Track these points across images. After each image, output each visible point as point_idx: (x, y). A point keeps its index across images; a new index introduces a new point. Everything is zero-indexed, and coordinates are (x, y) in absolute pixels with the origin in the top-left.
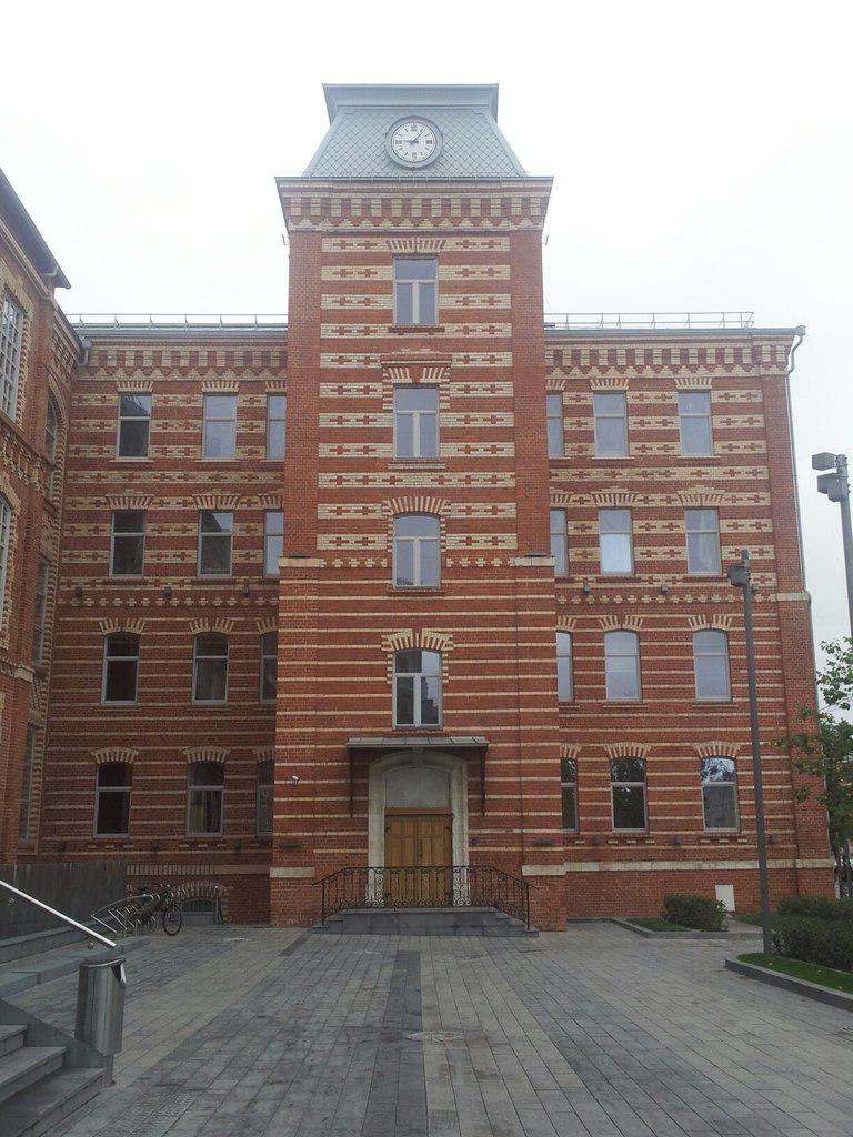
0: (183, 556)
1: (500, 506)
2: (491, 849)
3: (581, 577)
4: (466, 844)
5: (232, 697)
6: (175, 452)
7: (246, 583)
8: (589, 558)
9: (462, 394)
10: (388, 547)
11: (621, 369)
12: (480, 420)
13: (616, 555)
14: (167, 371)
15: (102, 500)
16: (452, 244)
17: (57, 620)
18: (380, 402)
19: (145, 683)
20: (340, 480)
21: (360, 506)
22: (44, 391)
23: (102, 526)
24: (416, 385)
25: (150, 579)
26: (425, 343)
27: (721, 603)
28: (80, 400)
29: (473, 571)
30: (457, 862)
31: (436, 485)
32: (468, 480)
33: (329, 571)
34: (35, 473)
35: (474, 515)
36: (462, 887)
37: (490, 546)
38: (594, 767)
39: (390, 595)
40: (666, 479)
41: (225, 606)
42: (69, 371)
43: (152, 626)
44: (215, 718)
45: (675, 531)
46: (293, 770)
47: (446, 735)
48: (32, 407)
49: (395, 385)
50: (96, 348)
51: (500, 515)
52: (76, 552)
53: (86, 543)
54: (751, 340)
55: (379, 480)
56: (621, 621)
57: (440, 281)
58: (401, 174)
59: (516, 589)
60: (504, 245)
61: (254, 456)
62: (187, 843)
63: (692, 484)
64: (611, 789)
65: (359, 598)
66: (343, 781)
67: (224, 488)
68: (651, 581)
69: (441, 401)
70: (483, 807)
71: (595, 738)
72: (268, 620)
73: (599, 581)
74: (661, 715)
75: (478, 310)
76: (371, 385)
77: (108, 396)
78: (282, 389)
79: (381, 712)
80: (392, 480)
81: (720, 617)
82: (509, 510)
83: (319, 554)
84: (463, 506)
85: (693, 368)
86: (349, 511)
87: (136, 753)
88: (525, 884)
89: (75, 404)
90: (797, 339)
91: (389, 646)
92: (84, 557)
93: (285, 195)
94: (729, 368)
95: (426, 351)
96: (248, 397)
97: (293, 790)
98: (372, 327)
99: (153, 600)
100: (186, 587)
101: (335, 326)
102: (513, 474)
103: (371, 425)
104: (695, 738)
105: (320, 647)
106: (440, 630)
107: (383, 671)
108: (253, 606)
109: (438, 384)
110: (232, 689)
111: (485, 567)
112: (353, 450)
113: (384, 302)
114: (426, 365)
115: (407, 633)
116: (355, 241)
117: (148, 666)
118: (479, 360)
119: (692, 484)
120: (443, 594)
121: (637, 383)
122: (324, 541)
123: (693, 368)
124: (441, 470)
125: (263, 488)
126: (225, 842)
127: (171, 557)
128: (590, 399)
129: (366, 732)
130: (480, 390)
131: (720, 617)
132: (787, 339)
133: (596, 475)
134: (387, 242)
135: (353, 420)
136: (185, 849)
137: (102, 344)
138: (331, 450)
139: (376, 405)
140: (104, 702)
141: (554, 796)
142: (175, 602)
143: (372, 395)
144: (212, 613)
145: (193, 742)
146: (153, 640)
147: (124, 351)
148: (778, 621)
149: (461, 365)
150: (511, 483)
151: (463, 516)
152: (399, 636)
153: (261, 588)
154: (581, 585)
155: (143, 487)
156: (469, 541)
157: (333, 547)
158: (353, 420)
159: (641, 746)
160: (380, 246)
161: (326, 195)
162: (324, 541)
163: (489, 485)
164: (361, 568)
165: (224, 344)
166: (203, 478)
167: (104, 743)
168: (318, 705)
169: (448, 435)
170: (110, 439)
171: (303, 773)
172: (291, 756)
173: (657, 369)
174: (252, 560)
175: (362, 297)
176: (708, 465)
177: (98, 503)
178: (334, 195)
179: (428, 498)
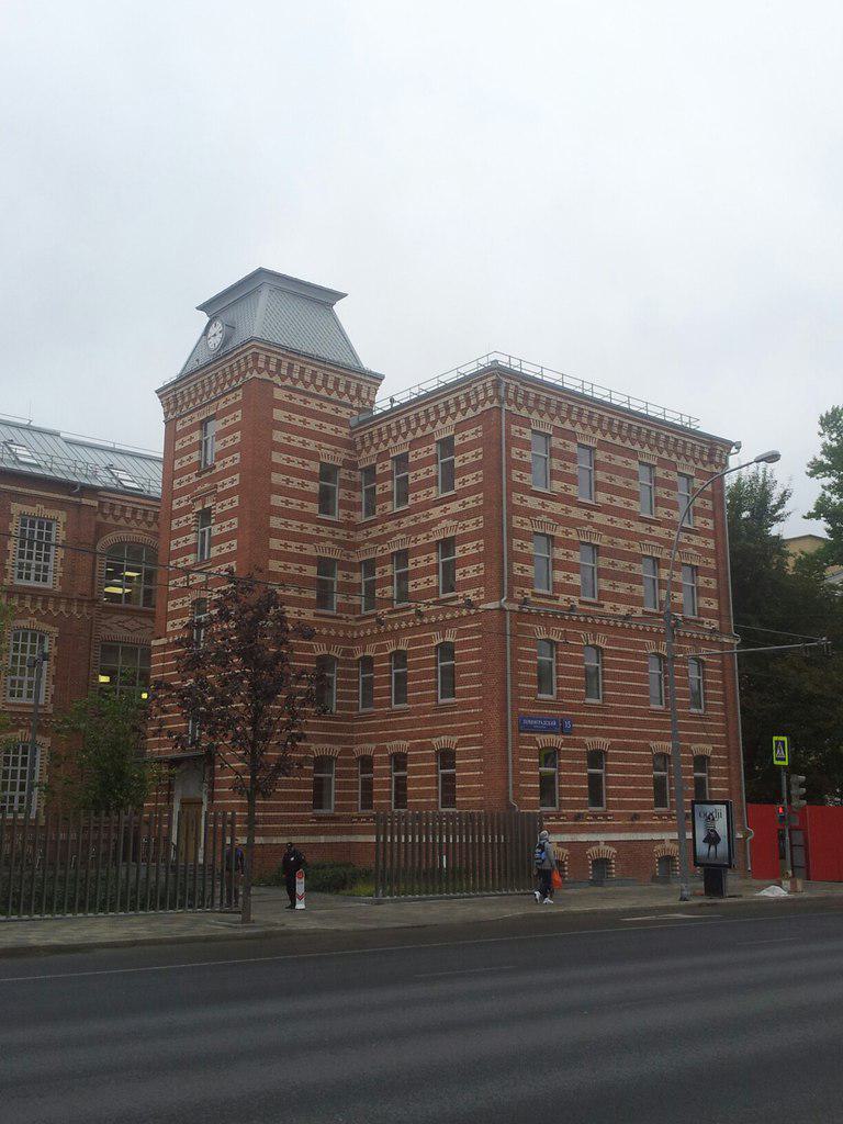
27: (452, 619)
43: (413, 642)
104: (433, 734)
117: (414, 675)
170: (343, 505)
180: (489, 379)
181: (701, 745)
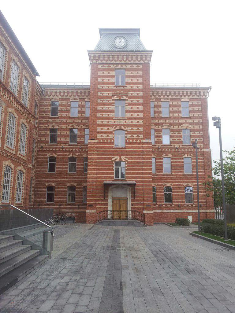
1: (139, 128)
3: (158, 145)
7: (81, 145)
9: (131, 102)
11: (168, 96)
12: (135, 108)
14: (62, 96)
16: (129, 67)
18: (112, 103)
19: (57, 168)
22: (34, 100)
24: (120, 100)
25: (59, 144)
26: (122, 90)
28: (42, 102)
29: (133, 143)
30: (128, 209)
31: (124, 123)
34: (32, 120)
35: (133, 130)
36: (130, 215)
37: (137, 137)
38: (160, 188)
39: (114, 148)
43: (59, 155)
51: (139, 130)
55: (111, 122)
56: (167, 155)
58: (117, 50)
59: (143, 147)
61: (82, 116)
63: (184, 123)
64: (164, 194)
66: (103, 191)
67: (75, 123)
71: (161, 182)
73: (162, 146)
76: (110, 100)
82: (141, 129)
83: (97, 139)
84: (131, 128)
85: (185, 96)
88: (144, 215)
89: (41, 103)
90: (209, 89)
92: (43, 139)
93: (90, 55)
95: (122, 92)
96: (81, 102)
97: (91, 193)
98: (110, 86)
100: (67, 146)
101: (101, 86)
104: (184, 182)
107: (112, 166)
108: (82, 151)
112: (105, 115)
113: (112, 80)
115: (117, 157)
118: (135, 94)
119: (184, 123)
120: (126, 148)
123: (185, 96)
127: (63, 139)
130: (135, 101)
132: (207, 90)
133: (162, 121)
134: (114, 66)
135: (105, 108)
139: (111, 104)
142: (64, 150)
143: (110, 102)
144: (72, 152)
145: (69, 182)
146: (59, 158)
149: (131, 95)
150: (142, 123)
151: (131, 130)
154: (158, 147)
155: (57, 123)
156: (132, 136)
157: (100, 137)
158: (105, 108)
160: (112, 67)
162: (98, 136)
163: (137, 123)
166: (71, 121)
171: (93, 189)
174: (82, 140)
175: (108, 79)
176: (188, 119)
178: (101, 55)
180: (54, 90)
181: (73, 183)
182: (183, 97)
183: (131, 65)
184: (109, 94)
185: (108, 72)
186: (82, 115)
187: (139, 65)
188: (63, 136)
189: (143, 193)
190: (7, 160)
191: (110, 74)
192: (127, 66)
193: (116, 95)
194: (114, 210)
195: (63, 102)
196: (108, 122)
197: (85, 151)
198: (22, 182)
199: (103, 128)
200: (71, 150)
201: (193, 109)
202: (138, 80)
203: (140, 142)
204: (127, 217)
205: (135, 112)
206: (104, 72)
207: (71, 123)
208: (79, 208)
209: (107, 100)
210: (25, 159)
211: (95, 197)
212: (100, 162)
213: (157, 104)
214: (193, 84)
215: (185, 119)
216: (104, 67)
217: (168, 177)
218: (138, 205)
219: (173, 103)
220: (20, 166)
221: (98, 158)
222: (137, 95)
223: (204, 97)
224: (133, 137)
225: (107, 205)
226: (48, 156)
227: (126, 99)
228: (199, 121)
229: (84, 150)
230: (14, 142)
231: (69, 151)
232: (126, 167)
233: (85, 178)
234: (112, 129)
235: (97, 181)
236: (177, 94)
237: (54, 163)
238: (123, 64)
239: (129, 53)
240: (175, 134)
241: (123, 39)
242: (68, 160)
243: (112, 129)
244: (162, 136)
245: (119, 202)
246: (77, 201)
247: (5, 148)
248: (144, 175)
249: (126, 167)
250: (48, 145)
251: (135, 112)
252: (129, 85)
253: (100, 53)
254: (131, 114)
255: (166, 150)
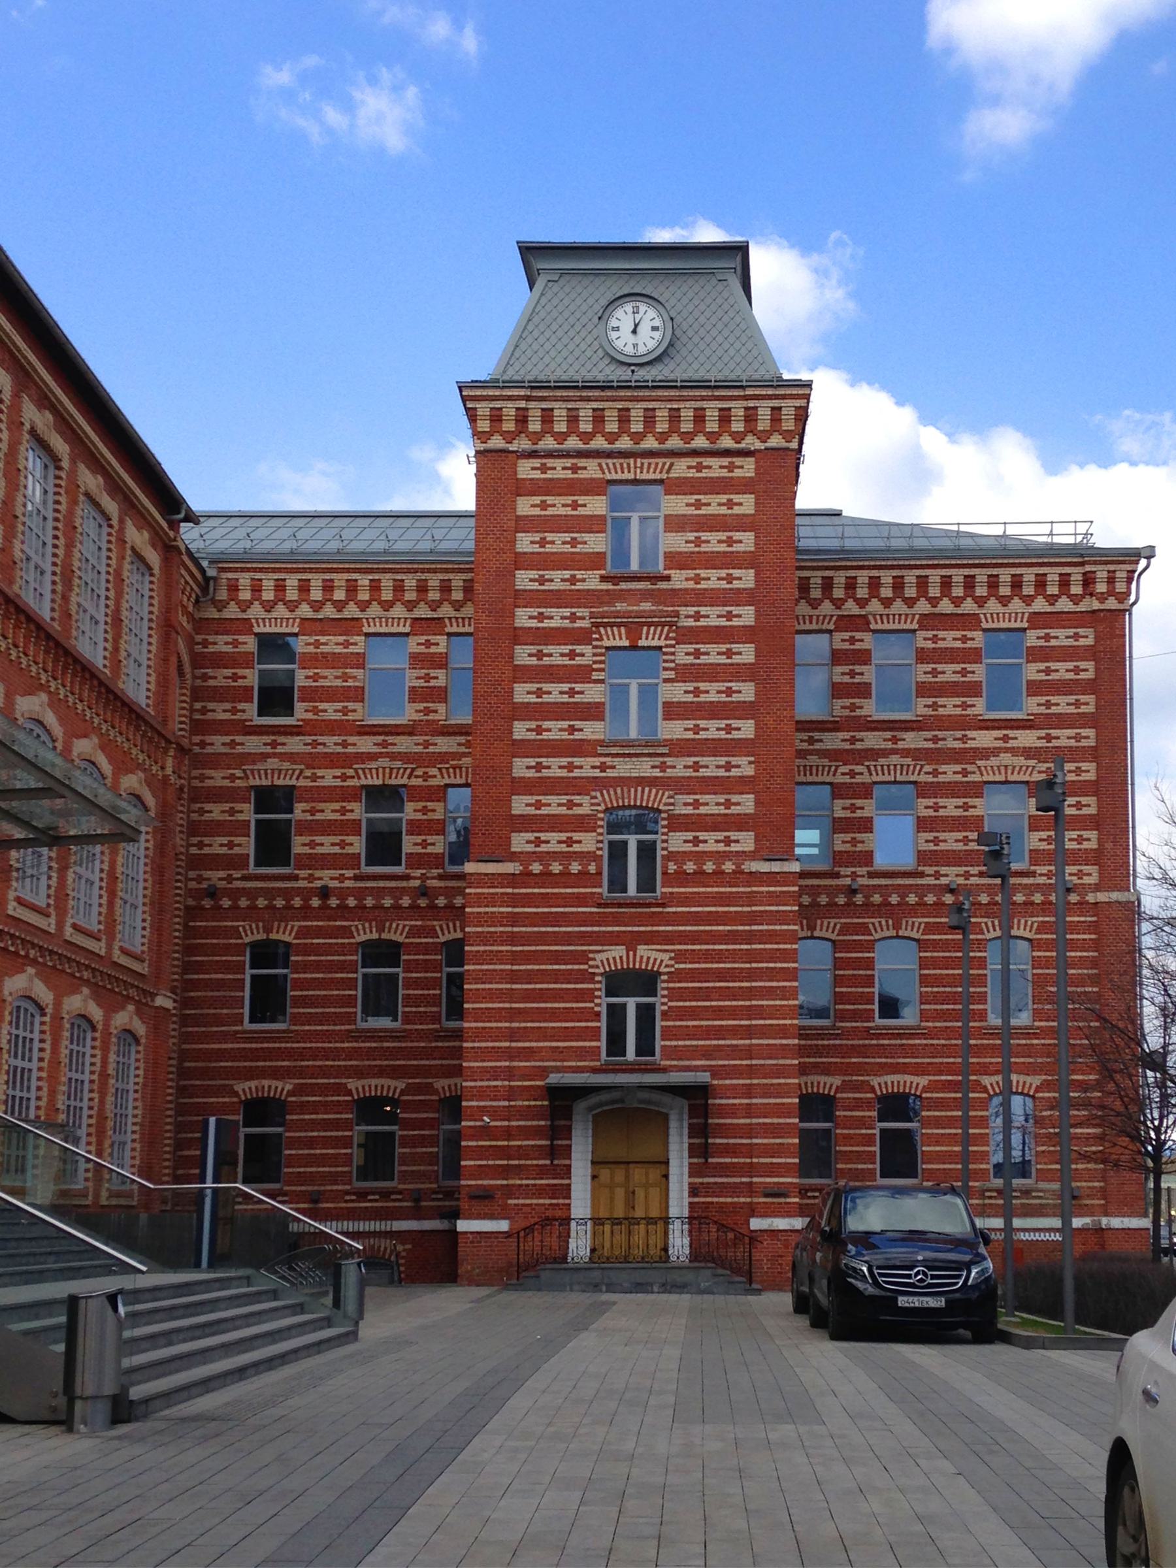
0: (342, 844)
1: (735, 798)
2: (715, 1200)
3: (849, 871)
4: (686, 1194)
5: (407, 1019)
6: (331, 711)
7: (423, 878)
8: (860, 847)
9: (690, 660)
10: (598, 849)
11: (910, 602)
12: (712, 692)
13: (893, 842)
14: (317, 606)
15: (238, 773)
16: (682, 468)
17: (186, 926)
18: (589, 669)
19: (298, 1002)
20: (539, 767)
21: (564, 799)
22: (174, 659)
23: (238, 806)
24: (634, 647)
25: (303, 873)
26: (646, 595)
27: (1025, 903)
28: (205, 644)
29: (700, 876)
30: (673, 1212)
31: (657, 773)
32: (696, 767)
33: (526, 877)
34: (169, 763)
35: (703, 810)
36: (679, 1243)
37: (721, 847)
38: (858, 1104)
39: (599, 905)
40: (962, 746)
41: (397, 907)
42: (191, 609)
44: (386, 1044)
45: (971, 812)
46: (483, 1110)
47: (664, 1070)
48: (163, 684)
49: (607, 648)
50: (224, 575)
51: (735, 810)
52: (207, 840)
53: (216, 828)
54: (1082, 564)
55: (587, 767)
56: (897, 927)
57: (666, 516)
58: (624, 374)
59: (751, 899)
60: (747, 468)
61: (431, 717)
62: (354, 1194)
63: (995, 752)
64: (877, 1132)
65: (561, 910)
66: (542, 1123)
67: (393, 757)
68: (937, 875)
69: (665, 669)
70: (706, 1152)
71: (859, 1069)
72: (451, 925)
73: (871, 875)
74: (943, 1042)
75: (712, 552)
76: (579, 649)
77: (241, 638)
78: (467, 629)
79: (587, 1044)
80: (603, 767)
81: (1023, 921)
82: (746, 804)
83: (513, 857)
84: (690, 799)
85: (1004, 601)
86: (549, 805)
87: (288, 1087)
88: (754, 1238)
89: (198, 648)
90: (1143, 562)
91: (597, 967)
92: (217, 845)
93: (469, 405)
94: (1051, 600)
95: (646, 606)
96: (422, 639)
97: (485, 1132)
98: (579, 574)
99: (306, 899)
100: (348, 884)
101: (534, 574)
102: (752, 759)
103: (578, 698)
105: (515, 967)
106: (659, 947)
107: (589, 995)
108: (432, 907)
109: (660, 648)
110: (407, 1009)
111: (715, 873)
112: (555, 730)
113: (595, 543)
114: (644, 624)
115: (618, 951)
116: (558, 463)
118: (713, 617)
119: (995, 752)
120: (663, 905)
121: (929, 621)
122: (520, 842)
123: (1004, 601)
124: (662, 755)
125: (443, 757)
126: (400, 1192)
127: (327, 845)
128: (867, 641)
129: (570, 1067)
130: (713, 655)
131: (1023, 921)
132: (1131, 562)
133: (873, 740)
134: (600, 465)
135: (555, 693)
136: (352, 1201)
137: (230, 570)
138: (528, 730)
139: (583, 674)
140: (247, 1025)
141: (790, 1141)
142: (334, 902)
143: (579, 661)
144: (379, 917)
145: (359, 1073)
146: (307, 950)
147: (260, 580)
148: (1093, 927)
149: (690, 623)
150: (749, 771)
151: (689, 810)
152: (610, 955)
153: (442, 884)
154: (848, 881)
155: (291, 757)
156: (696, 841)
157: (530, 848)
158: (555, 693)
159: (916, 1079)
160: (592, 469)
161: (523, 404)
162: (520, 842)
163: (722, 773)
164: (566, 874)
165: (390, 571)
166: (366, 744)
167: (250, 1074)
168: (512, 1035)
169: (673, 711)
171: (494, 1113)
172: (481, 1094)
173: (957, 602)
174: (430, 849)
175: (567, 537)
176: (1018, 728)
177: (233, 778)
178: (532, 405)
179: (647, 789)
181: (386, 1082)
182: (993, 605)
183: (693, 461)
184: (573, 618)
185: (569, 500)
186: (427, 711)
187: (738, 461)
188: (327, 828)
189: (749, 1131)
190: (75, 990)
191: (581, 511)
192: (672, 465)
193: (612, 625)
194: (603, 1214)
195: (323, 639)
196: (570, 767)
197: (450, 907)
198: (34, 1065)
199: (544, 799)
200: (369, 902)
201: (1048, 671)
202: (730, 542)
203: (738, 872)
204: (666, 1249)
205: (714, 711)
206: (550, 500)
207: (373, 757)
208: (417, 1213)
209: (566, 649)
210: (142, 968)
211: (504, 1152)
212: (530, 977)
213: (846, 646)
214: (1057, 529)
215: (999, 728)
216: (549, 475)
217: (898, 1042)
218: (723, 1189)
219: (935, 639)
220: (123, 1008)
221: (515, 958)
222: (723, 622)
223: (1111, 603)
224: (702, 847)
225: (566, 1191)
226: (247, 940)
227: (667, 646)
228: (1078, 738)
229: (441, 902)
230: (101, 897)
231: (360, 912)
232: (666, 1000)
233: (449, 1052)
234: (592, 804)
235: (510, 1074)
236: (958, 591)
237: (276, 976)
238: (651, 454)
239: (685, 393)
240: (942, 812)
241: (652, 313)
242: (358, 958)
243: (592, 804)
244: (869, 820)
245: (627, 1177)
246: (404, 1177)
247: (68, 931)
248: (754, 1041)
249: (666, 1000)
250: (244, 878)
251: (714, 711)
252: (681, 568)
253: (528, 399)
254: (690, 724)
255: (894, 899)
